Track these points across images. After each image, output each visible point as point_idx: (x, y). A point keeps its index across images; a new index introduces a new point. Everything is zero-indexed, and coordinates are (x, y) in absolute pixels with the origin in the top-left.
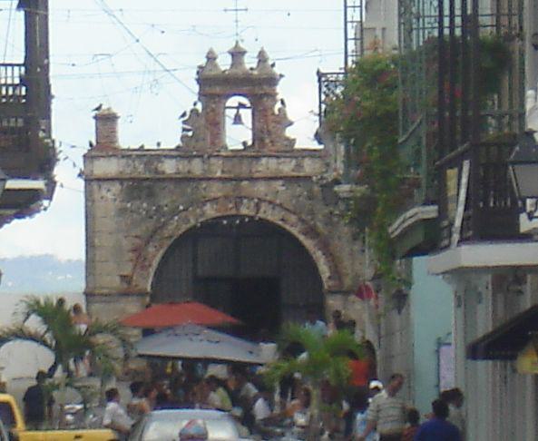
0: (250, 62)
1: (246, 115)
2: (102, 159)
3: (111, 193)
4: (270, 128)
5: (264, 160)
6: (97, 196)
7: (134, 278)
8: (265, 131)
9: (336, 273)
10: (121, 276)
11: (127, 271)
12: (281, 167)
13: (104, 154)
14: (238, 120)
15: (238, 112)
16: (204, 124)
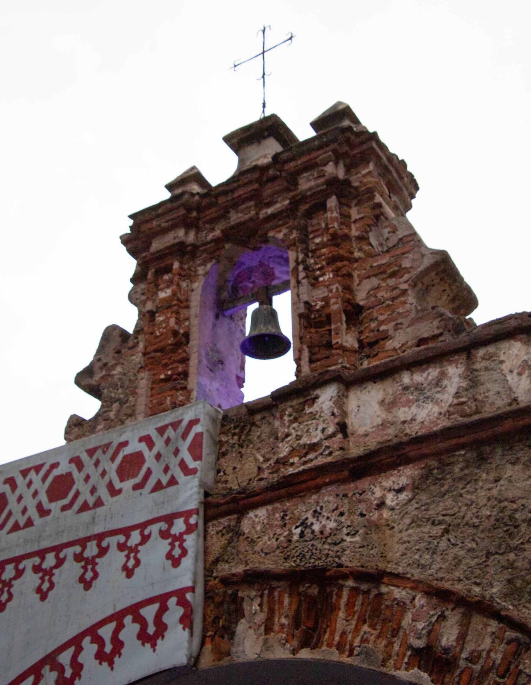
4: (361, 297)
12: (403, 413)
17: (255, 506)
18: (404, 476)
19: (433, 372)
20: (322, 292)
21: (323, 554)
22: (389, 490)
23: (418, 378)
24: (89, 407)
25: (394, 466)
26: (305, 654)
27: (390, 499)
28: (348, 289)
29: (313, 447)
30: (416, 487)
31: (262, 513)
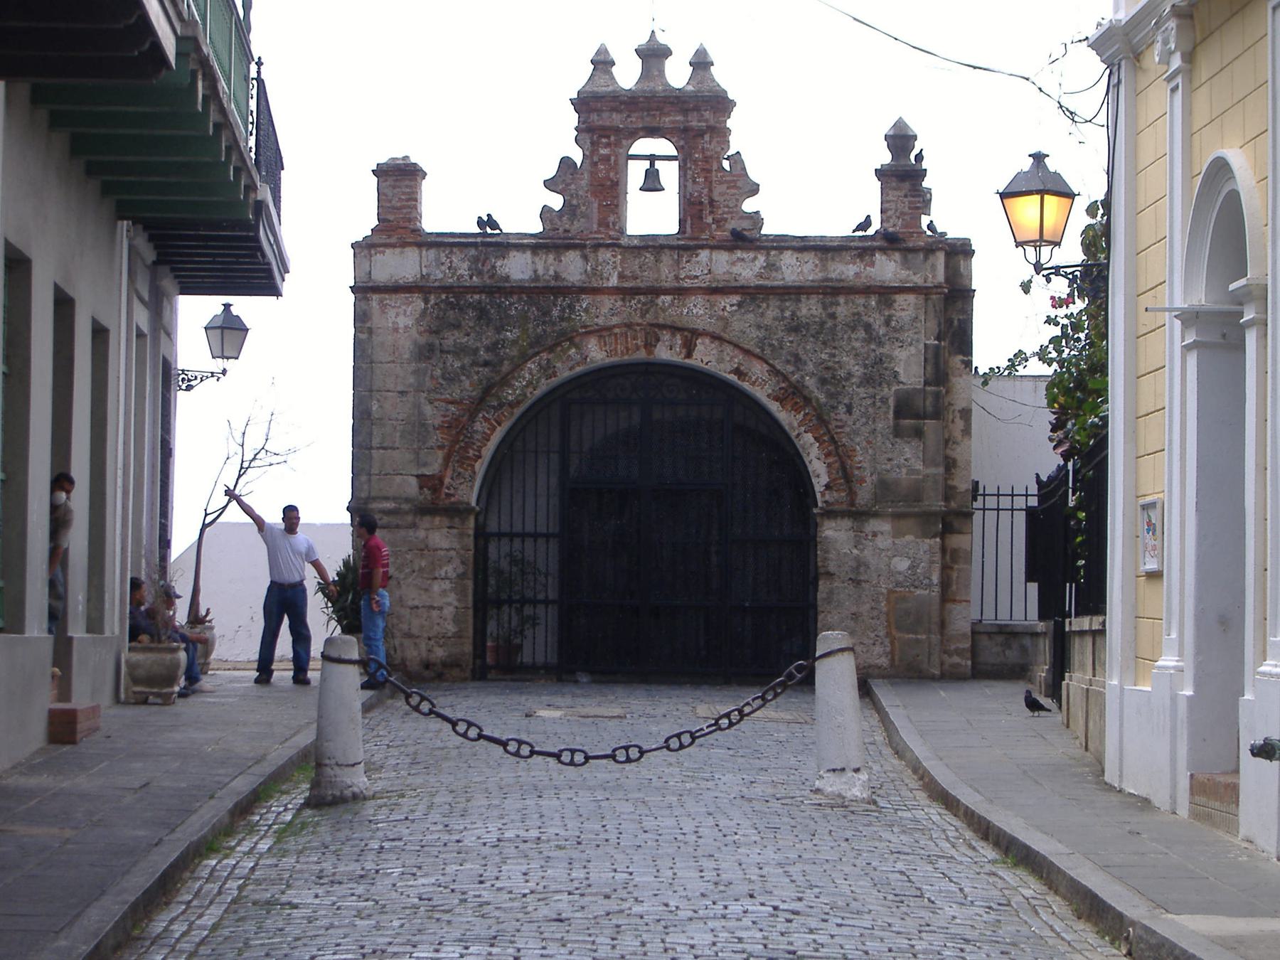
0: (677, 74)
1: (669, 173)
2: (388, 251)
3: (403, 318)
5: (704, 255)
6: (377, 320)
7: (447, 481)
8: (705, 200)
9: (845, 475)
10: (417, 476)
11: (433, 469)
12: (735, 270)
13: (393, 240)
14: (652, 183)
15: (652, 165)
16: (590, 187)
17: (665, 294)
18: (735, 299)
19: (751, 255)
20: (698, 188)
21: (700, 325)
22: (728, 303)
23: (745, 256)
24: (556, 201)
25: (731, 293)
26: (687, 361)
27: (728, 308)
28: (711, 191)
29: (696, 277)
30: (740, 305)
31: (668, 298)
